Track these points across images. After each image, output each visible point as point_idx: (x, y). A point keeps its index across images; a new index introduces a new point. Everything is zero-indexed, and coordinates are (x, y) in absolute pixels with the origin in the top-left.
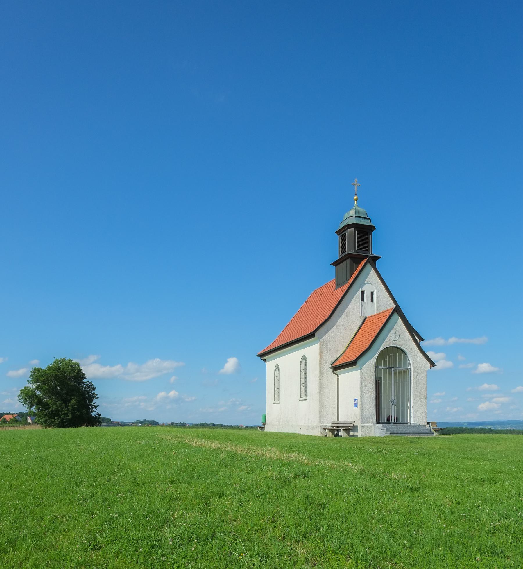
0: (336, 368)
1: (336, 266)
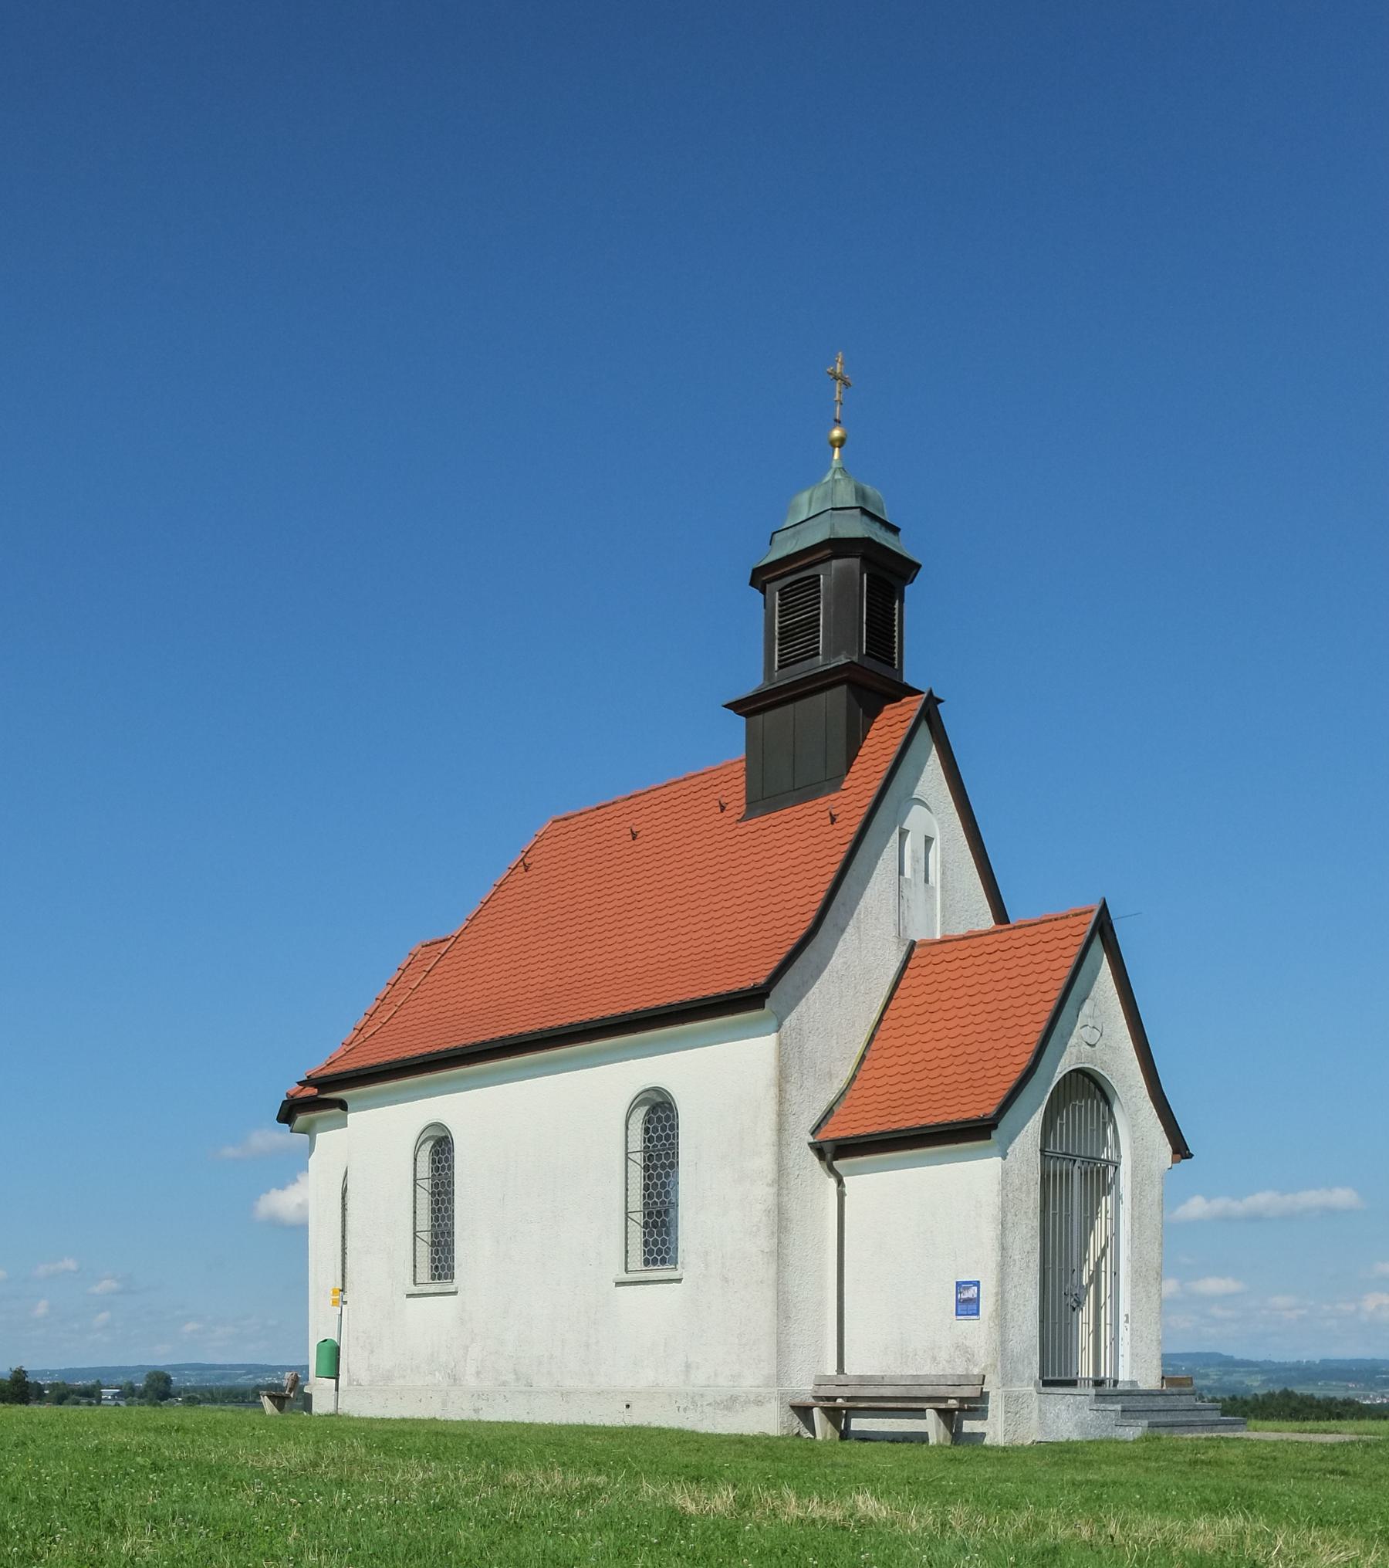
0: (838, 1150)
1: (746, 715)
